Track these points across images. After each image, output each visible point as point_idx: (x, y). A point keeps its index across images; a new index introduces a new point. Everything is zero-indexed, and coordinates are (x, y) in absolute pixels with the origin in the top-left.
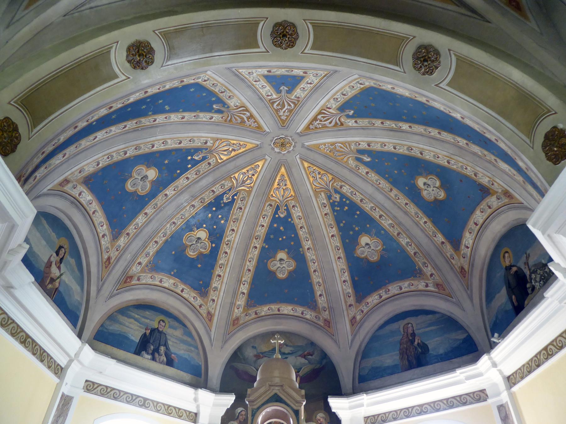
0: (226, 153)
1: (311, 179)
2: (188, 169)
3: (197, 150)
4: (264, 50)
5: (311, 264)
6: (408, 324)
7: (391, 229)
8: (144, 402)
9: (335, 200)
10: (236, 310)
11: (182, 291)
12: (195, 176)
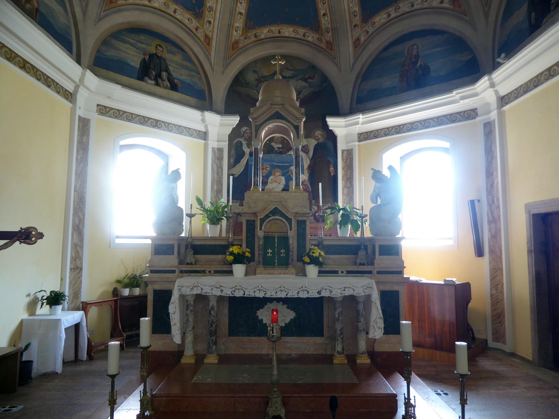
6: (414, 45)
10: (235, 33)
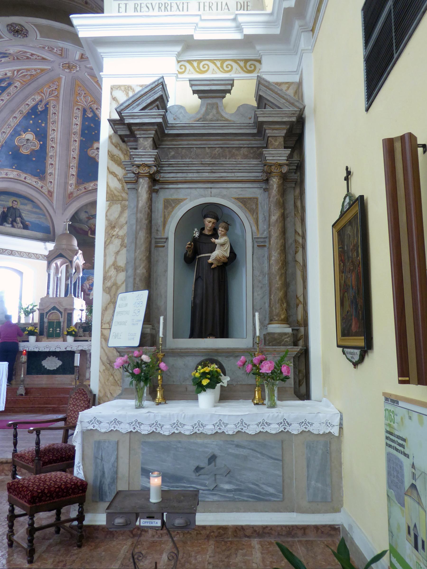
10: (70, 188)
11: (25, 178)
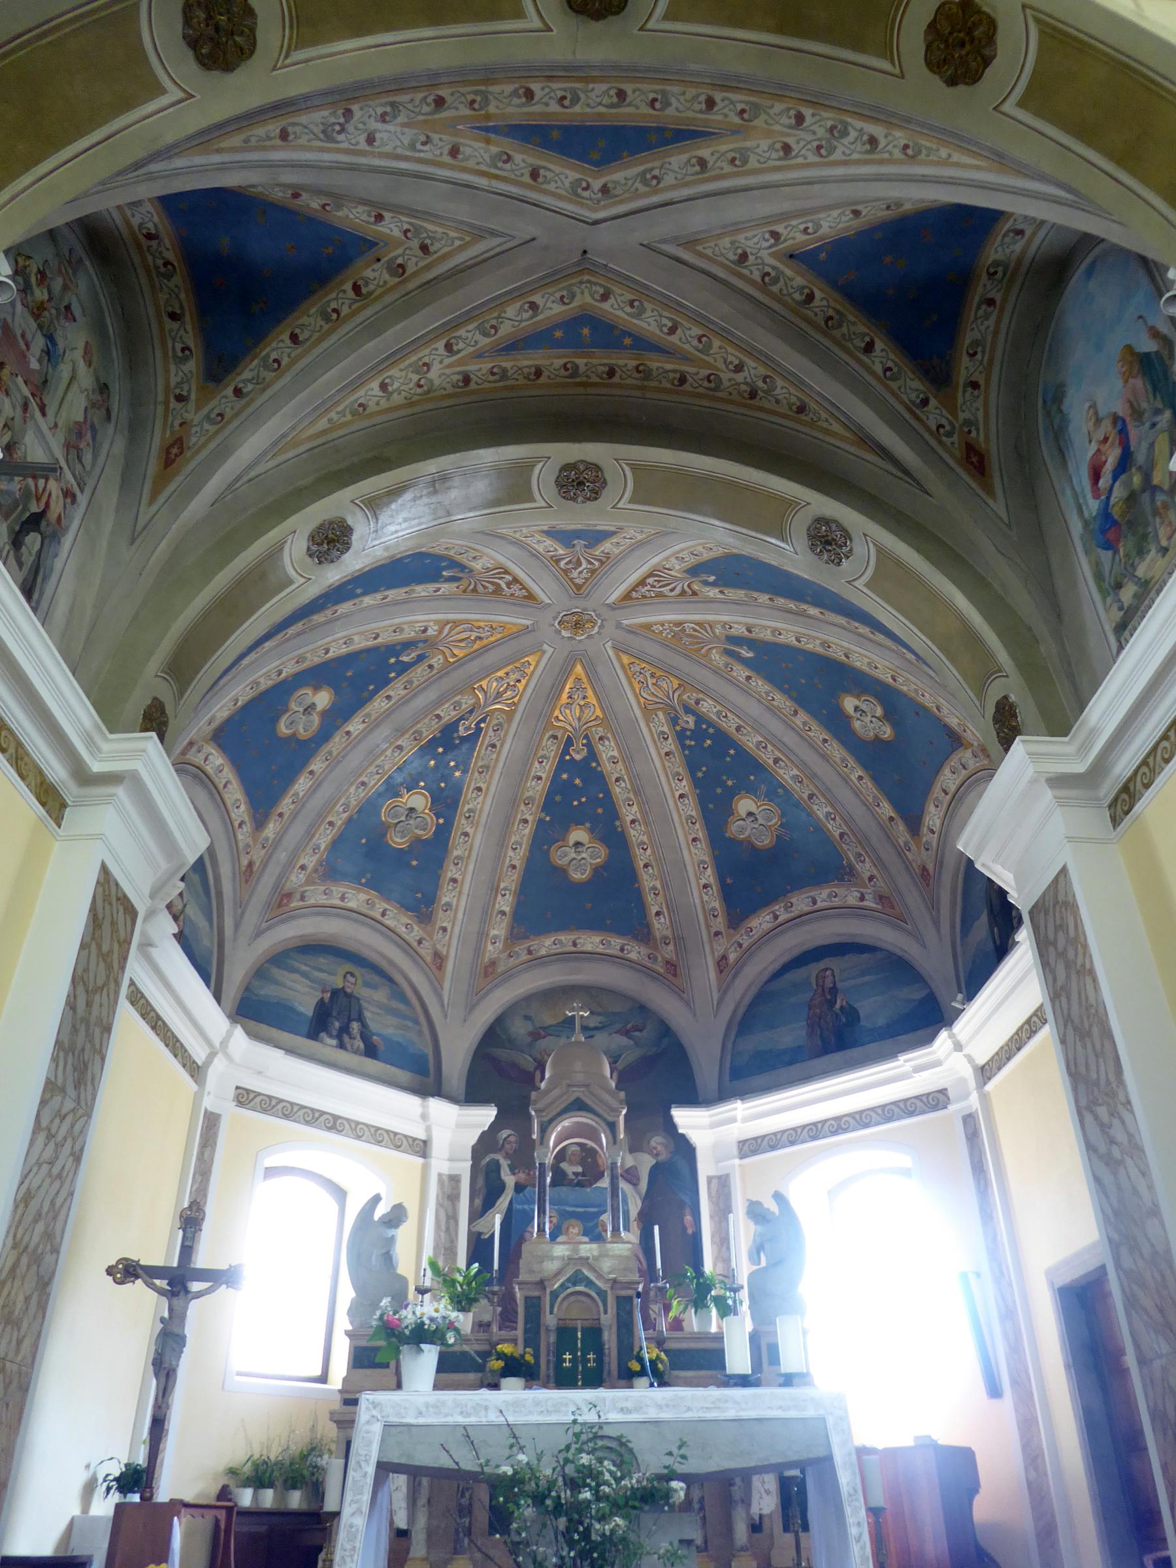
0: (462, 644)
1: (637, 686)
2: (388, 681)
3: (408, 645)
4: (544, 504)
5: (638, 852)
6: (826, 969)
7: (797, 786)
8: (335, 1123)
9: (686, 726)
10: (490, 947)
11: (383, 914)
12: (403, 692)
